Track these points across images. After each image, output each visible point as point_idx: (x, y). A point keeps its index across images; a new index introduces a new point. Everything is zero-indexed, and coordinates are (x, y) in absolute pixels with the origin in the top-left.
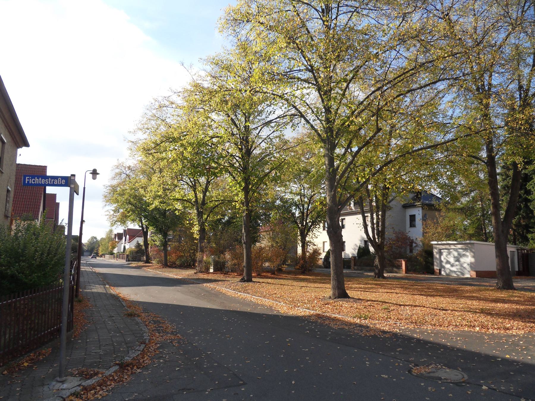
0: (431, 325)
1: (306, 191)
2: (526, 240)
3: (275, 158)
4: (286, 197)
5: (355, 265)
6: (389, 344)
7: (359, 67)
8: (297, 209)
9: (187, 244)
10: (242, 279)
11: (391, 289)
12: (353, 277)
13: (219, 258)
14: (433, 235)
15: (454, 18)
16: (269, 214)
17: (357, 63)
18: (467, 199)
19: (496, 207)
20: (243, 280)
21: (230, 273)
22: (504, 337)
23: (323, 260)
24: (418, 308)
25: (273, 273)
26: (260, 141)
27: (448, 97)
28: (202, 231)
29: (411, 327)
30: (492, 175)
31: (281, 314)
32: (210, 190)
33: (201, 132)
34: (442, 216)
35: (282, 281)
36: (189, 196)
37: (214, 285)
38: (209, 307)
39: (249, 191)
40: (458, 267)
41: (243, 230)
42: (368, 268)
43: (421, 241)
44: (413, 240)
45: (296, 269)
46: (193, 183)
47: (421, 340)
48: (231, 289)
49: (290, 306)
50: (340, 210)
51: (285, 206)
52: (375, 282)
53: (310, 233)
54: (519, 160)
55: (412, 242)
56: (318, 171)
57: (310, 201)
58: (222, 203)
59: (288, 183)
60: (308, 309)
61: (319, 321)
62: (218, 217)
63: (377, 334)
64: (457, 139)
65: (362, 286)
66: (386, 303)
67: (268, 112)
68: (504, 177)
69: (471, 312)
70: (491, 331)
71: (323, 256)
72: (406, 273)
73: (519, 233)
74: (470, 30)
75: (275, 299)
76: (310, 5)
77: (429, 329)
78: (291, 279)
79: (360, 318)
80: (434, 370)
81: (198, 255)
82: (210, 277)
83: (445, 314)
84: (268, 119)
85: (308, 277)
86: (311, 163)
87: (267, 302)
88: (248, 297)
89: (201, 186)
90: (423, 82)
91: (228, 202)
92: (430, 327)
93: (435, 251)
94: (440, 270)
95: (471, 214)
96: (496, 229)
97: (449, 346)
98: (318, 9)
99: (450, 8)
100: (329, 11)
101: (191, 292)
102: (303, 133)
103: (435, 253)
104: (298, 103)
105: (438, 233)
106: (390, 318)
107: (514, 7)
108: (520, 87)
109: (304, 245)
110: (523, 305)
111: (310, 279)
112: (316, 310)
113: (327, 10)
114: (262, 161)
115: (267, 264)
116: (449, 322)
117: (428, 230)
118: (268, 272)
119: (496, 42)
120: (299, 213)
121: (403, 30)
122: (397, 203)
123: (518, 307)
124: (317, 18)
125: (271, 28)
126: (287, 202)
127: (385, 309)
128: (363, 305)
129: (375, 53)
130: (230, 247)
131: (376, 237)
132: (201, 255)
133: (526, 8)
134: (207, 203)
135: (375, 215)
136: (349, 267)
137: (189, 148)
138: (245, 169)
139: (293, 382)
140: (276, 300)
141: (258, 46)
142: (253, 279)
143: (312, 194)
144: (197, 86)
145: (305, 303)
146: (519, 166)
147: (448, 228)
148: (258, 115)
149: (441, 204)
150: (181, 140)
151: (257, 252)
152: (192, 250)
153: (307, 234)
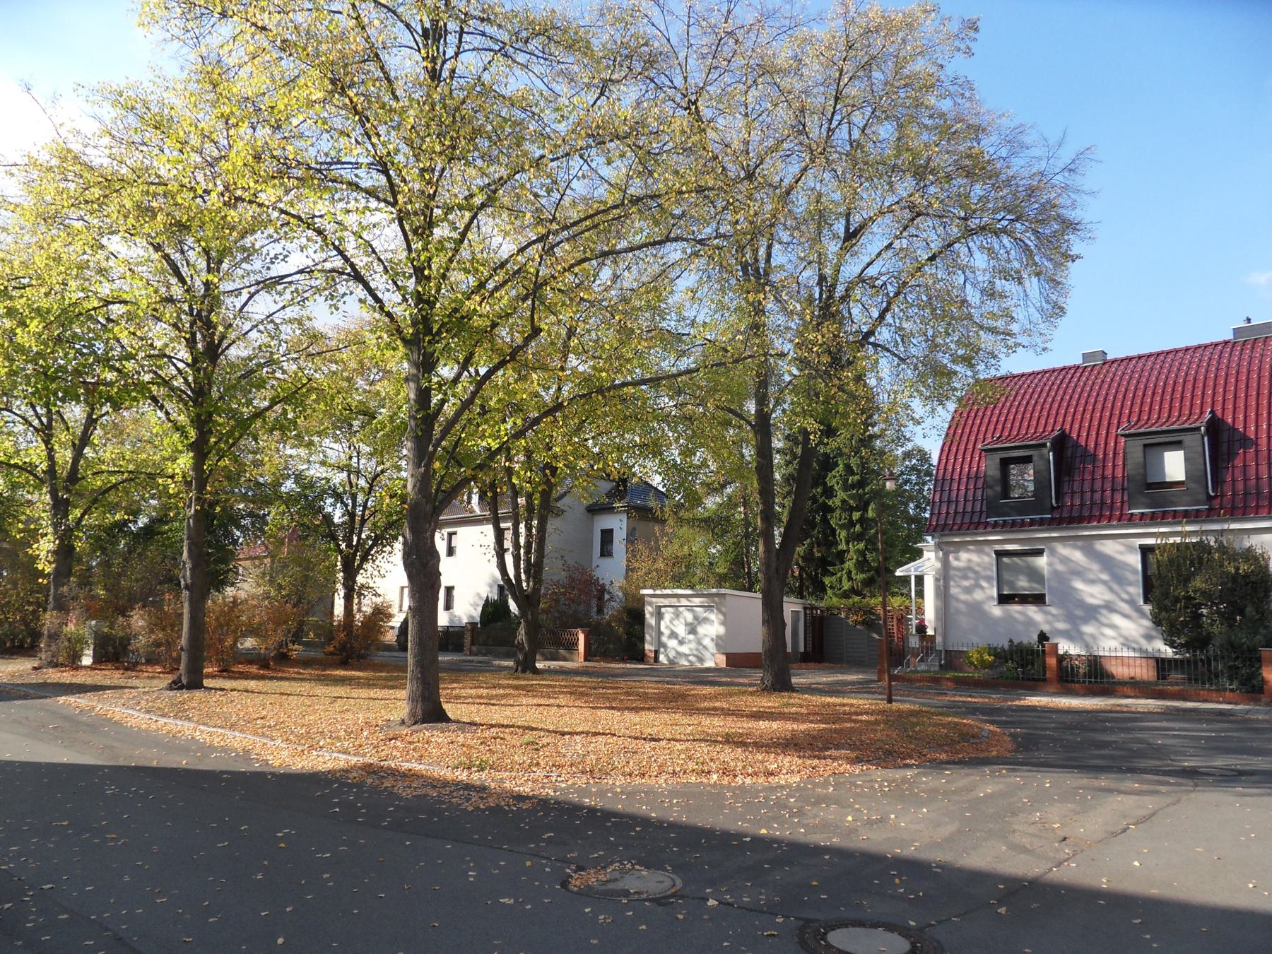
0: (624, 774)
1: (363, 461)
2: (820, 589)
3: (284, 372)
4: (312, 472)
5: (473, 643)
6: (526, 824)
7: (501, 181)
8: (339, 505)
9: (15, 587)
10: (174, 682)
11: (549, 698)
12: (465, 670)
13: (111, 627)
14: (647, 574)
15: (706, 113)
16: (265, 515)
17: (499, 171)
18: (718, 500)
19: (769, 517)
20: (176, 685)
21: (143, 668)
22: (761, 791)
23: (396, 632)
24: (600, 738)
25: (265, 666)
26: (247, 326)
27: (687, 281)
28: (65, 553)
29: (580, 784)
30: (764, 452)
31: (272, 770)
32: (96, 442)
33: (73, 284)
34: (667, 534)
35: (287, 683)
36: (27, 455)
37: (90, 700)
38: (65, 760)
39: (209, 452)
40: (693, 645)
41: (185, 554)
42: (504, 649)
43: (621, 588)
44: (604, 585)
45: (326, 654)
46: (44, 420)
47: (597, 810)
48: (140, 710)
49: (300, 748)
50: (437, 511)
51: (306, 497)
52: (515, 682)
53: (368, 566)
54: (811, 425)
55: (602, 590)
56: (395, 414)
57: (371, 486)
58: (131, 480)
59: (316, 439)
60: (344, 753)
61: (369, 781)
62: (118, 517)
63: (503, 803)
64: (698, 370)
65: (485, 692)
66: (533, 729)
67: (268, 254)
68: (788, 458)
69: (707, 741)
70: (739, 780)
71: (396, 622)
72: (586, 660)
73: (809, 575)
74: (736, 145)
75: (260, 731)
76: (394, 12)
77: (618, 784)
78: (310, 680)
79: (469, 768)
80: (617, 875)
81: (49, 619)
82: (80, 678)
83: (654, 749)
84: (273, 273)
85: (354, 673)
86: (378, 393)
87: (238, 740)
88: (186, 729)
89: (68, 429)
90: (638, 239)
91: (146, 477)
92: (620, 781)
93: (648, 610)
94: (657, 653)
95: (725, 532)
96: (767, 564)
97: (653, 818)
98: (413, 25)
99: (700, 91)
100: (440, 37)
101: (14, 721)
102: (362, 319)
103: (647, 616)
104: (350, 246)
105: (656, 570)
106: (538, 764)
107: (816, 117)
108: (822, 279)
109: (351, 592)
110: (804, 722)
111: (359, 678)
112: (364, 755)
113: (434, 34)
114: (249, 377)
115: (249, 643)
116: (660, 767)
117: (637, 565)
118: (251, 662)
119: (781, 180)
120: (343, 516)
121: (597, 115)
122: (575, 500)
123: (795, 726)
124: (411, 48)
125: (285, 45)
126: (311, 485)
127: (528, 744)
128: (479, 738)
129: (537, 155)
130: (146, 598)
131: (523, 576)
132: (57, 618)
133: (835, 123)
134: (83, 478)
135: (522, 526)
136: (458, 648)
137: (35, 322)
138: (200, 393)
139: (280, 941)
140: (263, 735)
141: (248, 82)
142: (206, 682)
143: (379, 469)
144: (67, 156)
145: (339, 739)
146: (812, 437)
147: (677, 561)
148: (246, 260)
149: (667, 509)
150: (11, 298)
151: (222, 611)
152: (30, 603)
153: (360, 567)
